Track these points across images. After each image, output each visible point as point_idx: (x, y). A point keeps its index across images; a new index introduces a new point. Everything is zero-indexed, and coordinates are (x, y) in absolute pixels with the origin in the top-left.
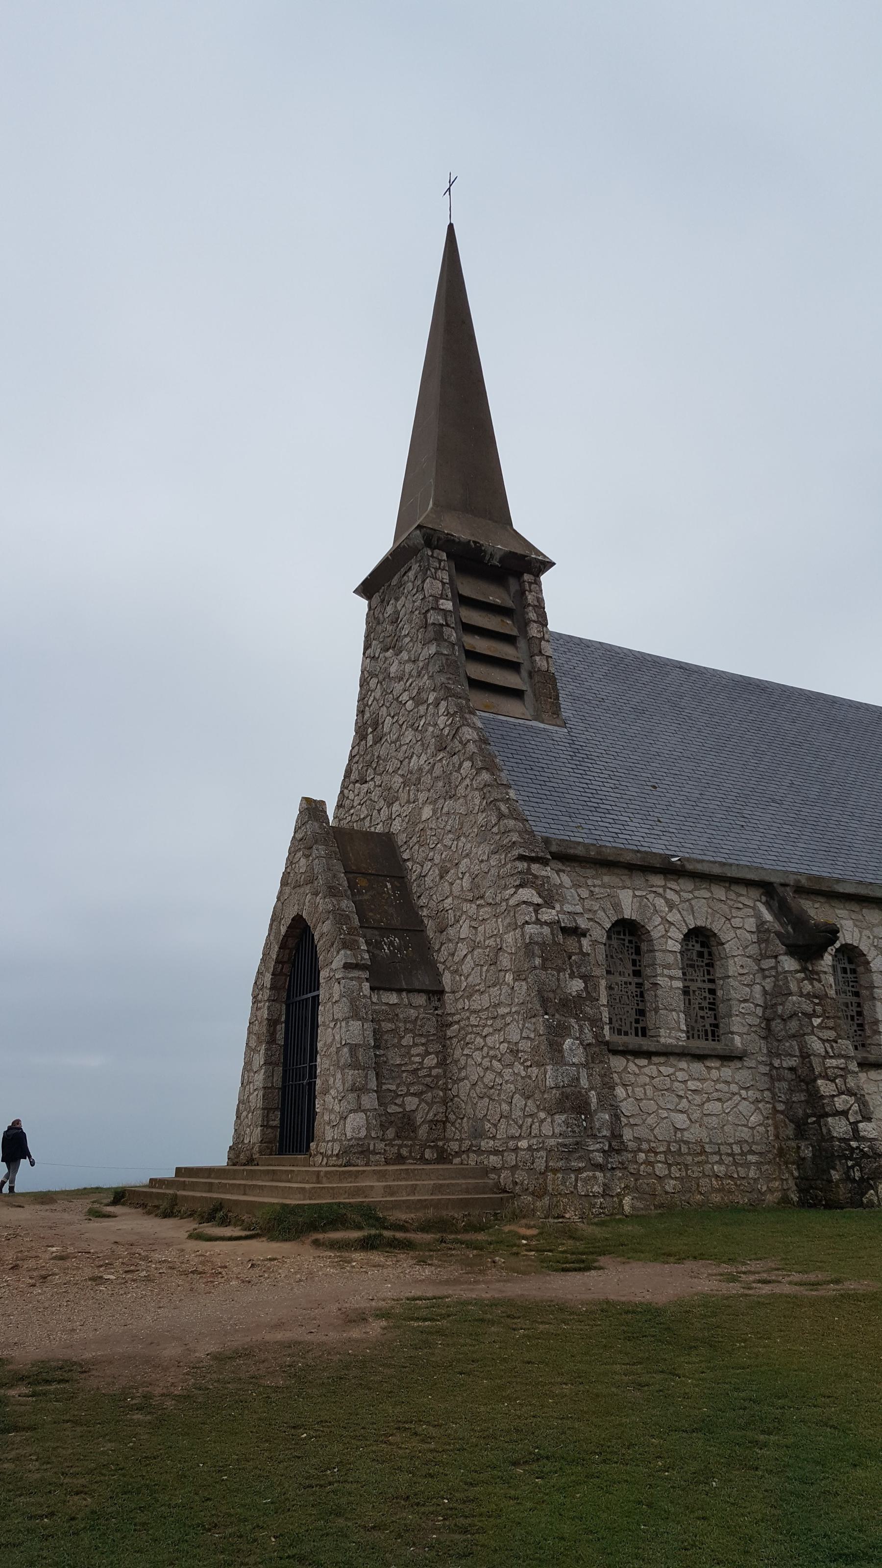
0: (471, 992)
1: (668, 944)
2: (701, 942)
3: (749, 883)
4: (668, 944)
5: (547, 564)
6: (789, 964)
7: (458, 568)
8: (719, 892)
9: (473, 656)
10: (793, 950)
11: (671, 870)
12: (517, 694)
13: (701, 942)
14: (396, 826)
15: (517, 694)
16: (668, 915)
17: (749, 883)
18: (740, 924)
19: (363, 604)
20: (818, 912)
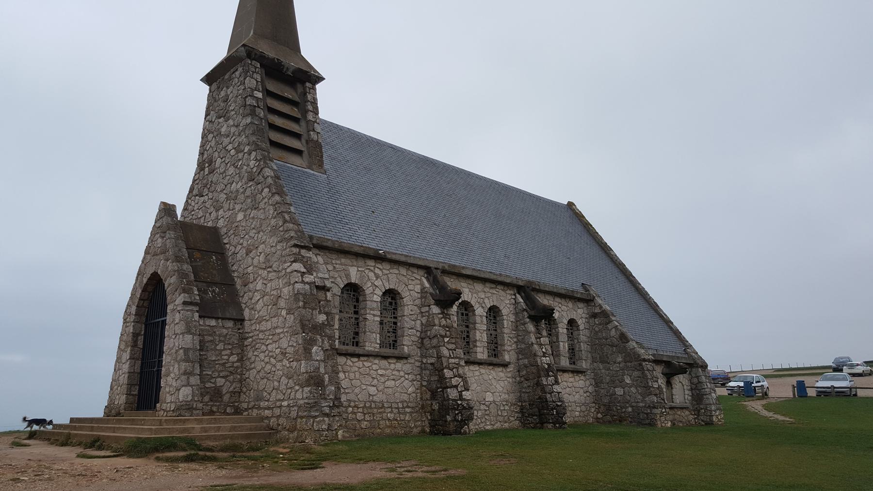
0: (260, 321)
1: (374, 297)
2: (392, 296)
3: (419, 267)
4: (374, 297)
5: (320, 79)
6: (435, 310)
7: (265, 79)
8: (403, 271)
9: (273, 127)
10: (438, 303)
11: (379, 258)
12: (299, 152)
13: (392, 296)
14: (221, 223)
15: (299, 152)
16: (375, 281)
17: (419, 267)
18: (413, 288)
19: (206, 88)
20: (452, 283)
